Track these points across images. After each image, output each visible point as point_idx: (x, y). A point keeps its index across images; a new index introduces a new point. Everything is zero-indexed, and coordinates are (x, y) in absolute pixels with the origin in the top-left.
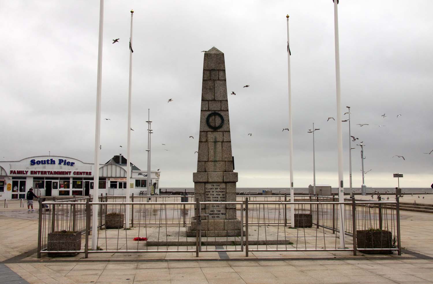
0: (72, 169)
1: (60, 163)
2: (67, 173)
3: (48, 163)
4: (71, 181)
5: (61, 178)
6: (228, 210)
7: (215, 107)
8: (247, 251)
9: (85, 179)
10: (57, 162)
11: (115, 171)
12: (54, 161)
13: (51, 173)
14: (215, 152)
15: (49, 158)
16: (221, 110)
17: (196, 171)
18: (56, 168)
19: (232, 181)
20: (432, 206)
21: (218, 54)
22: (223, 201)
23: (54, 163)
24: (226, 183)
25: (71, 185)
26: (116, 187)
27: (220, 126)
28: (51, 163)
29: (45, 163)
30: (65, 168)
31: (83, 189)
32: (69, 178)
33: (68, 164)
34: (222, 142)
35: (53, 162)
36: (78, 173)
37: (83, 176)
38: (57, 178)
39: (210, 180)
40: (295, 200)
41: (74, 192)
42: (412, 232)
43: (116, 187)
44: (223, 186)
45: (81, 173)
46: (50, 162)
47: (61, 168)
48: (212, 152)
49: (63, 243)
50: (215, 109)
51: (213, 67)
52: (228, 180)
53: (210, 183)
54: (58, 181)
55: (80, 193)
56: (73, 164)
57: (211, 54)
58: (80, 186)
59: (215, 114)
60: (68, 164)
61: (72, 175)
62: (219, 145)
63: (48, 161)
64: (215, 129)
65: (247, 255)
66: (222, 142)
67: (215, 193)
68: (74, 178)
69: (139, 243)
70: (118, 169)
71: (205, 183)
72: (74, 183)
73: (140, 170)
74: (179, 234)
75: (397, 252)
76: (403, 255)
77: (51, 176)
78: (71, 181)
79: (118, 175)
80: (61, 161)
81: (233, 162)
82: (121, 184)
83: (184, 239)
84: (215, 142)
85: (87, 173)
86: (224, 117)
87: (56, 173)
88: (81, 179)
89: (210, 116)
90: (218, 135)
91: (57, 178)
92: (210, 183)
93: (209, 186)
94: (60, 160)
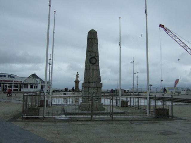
0: (14, 80)
1: (8, 77)
2: (11, 81)
3: (3, 77)
4: (13, 85)
5: (9, 84)
6: (98, 99)
7: (93, 55)
8: (112, 117)
9: (19, 84)
10: (7, 76)
11: (33, 81)
12: (6, 76)
13: (4, 81)
14: (93, 74)
15: (4, 75)
16: (96, 56)
17: (83, 82)
18: (7, 79)
19: (100, 86)
20: (190, 100)
21: (94, 32)
22: (96, 95)
23: (6, 77)
24: (97, 87)
25: (13, 87)
26: (33, 88)
27: (95, 63)
28: (4, 77)
29: (2, 77)
30: (11, 79)
31: (18, 89)
32: (12, 84)
33: (12, 77)
34: (96, 70)
35: (5, 76)
36: (16, 81)
37: (18, 83)
38: (7, 83)
39: (91, 86)
40: (121, 95)
41: (14, 90)
42: (178, 109)
43: (33, 88)
44: (96, 89)
45: (17, 81)
46: (4, 76)
47: (9, 79)
48: (91, 74)
49: (33, 113)
50: (93, 55)
51: (92, 38)
52: (98, 86)
53: (91, 87)
54: (7, 85)
55: (17, 90)
56: (14, 77)
57: (92, 32)
58: (17, 87)
59: (93, 58)
60: (12, 77)
61: (13, 82)
62: (94, 71)
63: (3, 75)
64: (93, 64)
65: (112, 119)
66: (96, 70)
67: (93, 92)
68: (14, 84)
69: (52, 111)
70: (34, 80)
71: (89, 87)
72: (14, 86)
73: (42, 80)
74: (75, 109)
75: (171, 117)
76: (173, 119)
77: (4, 82)
78: (13, 85)
79: (34, 83)
80: (9, 76)
81: (100, 78)
82: (35, 87)
83: (77, 111)
84: (93, 70)
85: (20, 81)
86: (97, 59)
87: (6, 81)
88: (17, 84)
89: (91, 58)
90: (94, 67)
91: (7, 83)
92: (91, 87)
93: (90, 89)
94: (8, 75)
